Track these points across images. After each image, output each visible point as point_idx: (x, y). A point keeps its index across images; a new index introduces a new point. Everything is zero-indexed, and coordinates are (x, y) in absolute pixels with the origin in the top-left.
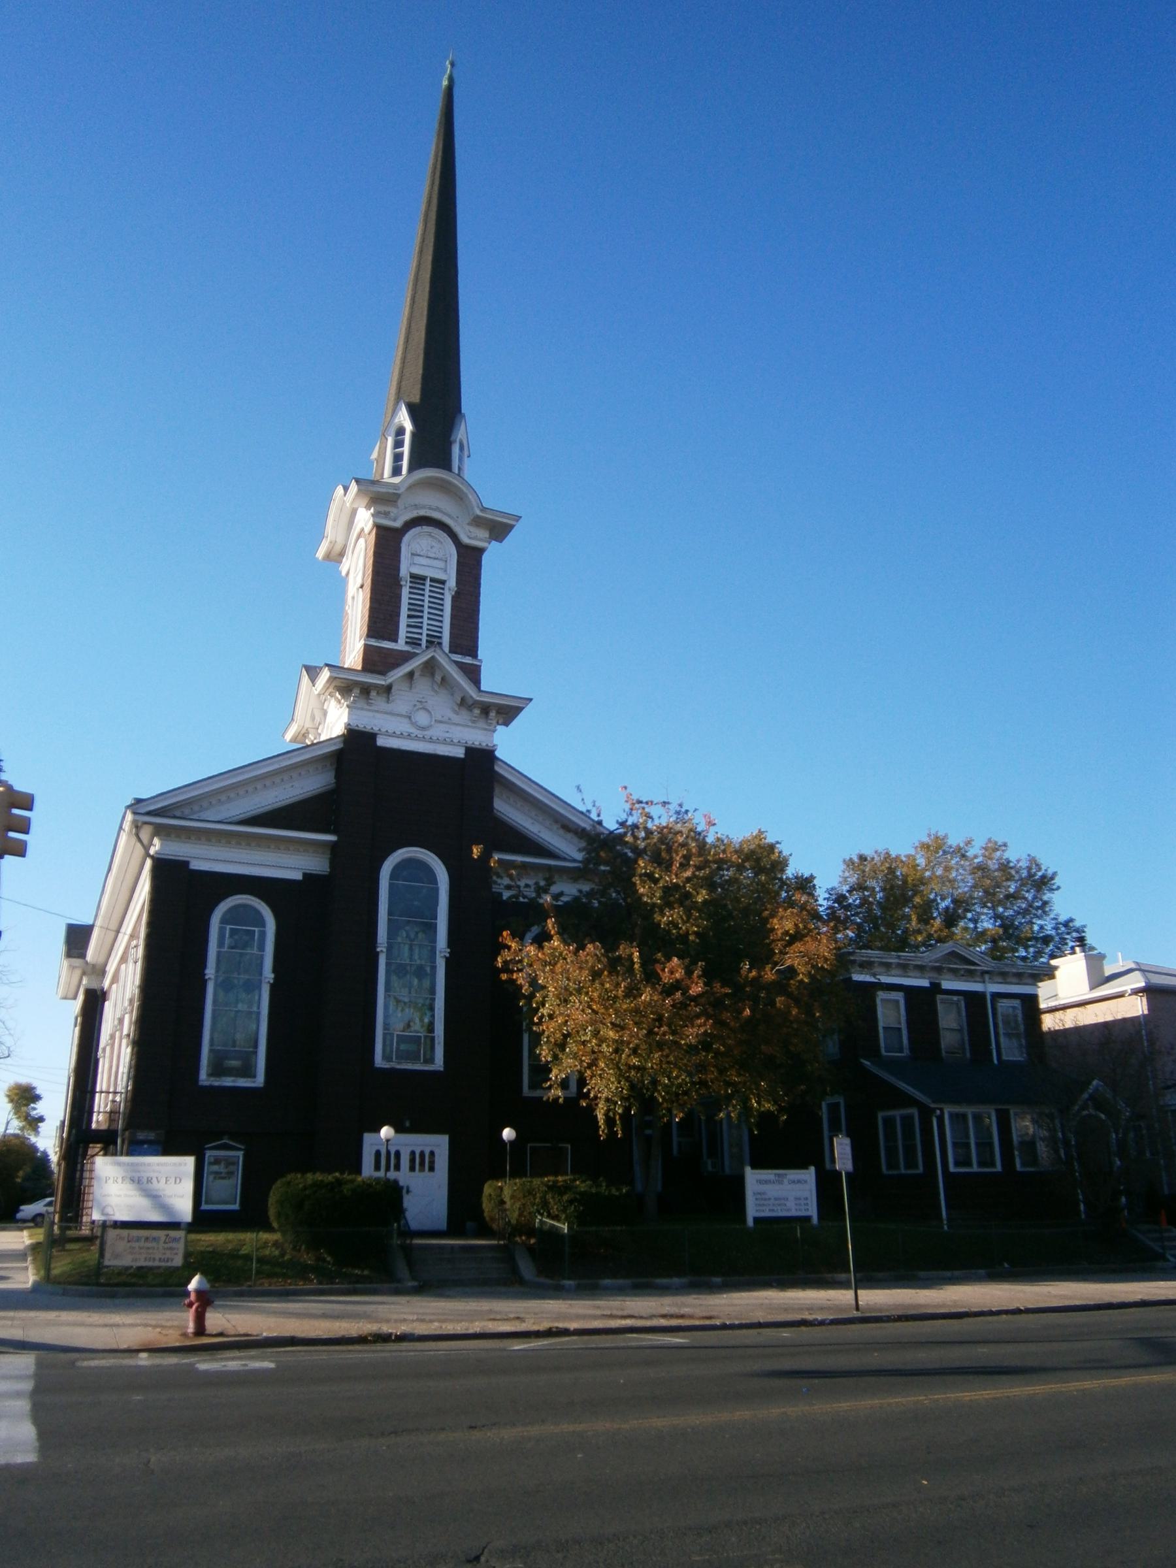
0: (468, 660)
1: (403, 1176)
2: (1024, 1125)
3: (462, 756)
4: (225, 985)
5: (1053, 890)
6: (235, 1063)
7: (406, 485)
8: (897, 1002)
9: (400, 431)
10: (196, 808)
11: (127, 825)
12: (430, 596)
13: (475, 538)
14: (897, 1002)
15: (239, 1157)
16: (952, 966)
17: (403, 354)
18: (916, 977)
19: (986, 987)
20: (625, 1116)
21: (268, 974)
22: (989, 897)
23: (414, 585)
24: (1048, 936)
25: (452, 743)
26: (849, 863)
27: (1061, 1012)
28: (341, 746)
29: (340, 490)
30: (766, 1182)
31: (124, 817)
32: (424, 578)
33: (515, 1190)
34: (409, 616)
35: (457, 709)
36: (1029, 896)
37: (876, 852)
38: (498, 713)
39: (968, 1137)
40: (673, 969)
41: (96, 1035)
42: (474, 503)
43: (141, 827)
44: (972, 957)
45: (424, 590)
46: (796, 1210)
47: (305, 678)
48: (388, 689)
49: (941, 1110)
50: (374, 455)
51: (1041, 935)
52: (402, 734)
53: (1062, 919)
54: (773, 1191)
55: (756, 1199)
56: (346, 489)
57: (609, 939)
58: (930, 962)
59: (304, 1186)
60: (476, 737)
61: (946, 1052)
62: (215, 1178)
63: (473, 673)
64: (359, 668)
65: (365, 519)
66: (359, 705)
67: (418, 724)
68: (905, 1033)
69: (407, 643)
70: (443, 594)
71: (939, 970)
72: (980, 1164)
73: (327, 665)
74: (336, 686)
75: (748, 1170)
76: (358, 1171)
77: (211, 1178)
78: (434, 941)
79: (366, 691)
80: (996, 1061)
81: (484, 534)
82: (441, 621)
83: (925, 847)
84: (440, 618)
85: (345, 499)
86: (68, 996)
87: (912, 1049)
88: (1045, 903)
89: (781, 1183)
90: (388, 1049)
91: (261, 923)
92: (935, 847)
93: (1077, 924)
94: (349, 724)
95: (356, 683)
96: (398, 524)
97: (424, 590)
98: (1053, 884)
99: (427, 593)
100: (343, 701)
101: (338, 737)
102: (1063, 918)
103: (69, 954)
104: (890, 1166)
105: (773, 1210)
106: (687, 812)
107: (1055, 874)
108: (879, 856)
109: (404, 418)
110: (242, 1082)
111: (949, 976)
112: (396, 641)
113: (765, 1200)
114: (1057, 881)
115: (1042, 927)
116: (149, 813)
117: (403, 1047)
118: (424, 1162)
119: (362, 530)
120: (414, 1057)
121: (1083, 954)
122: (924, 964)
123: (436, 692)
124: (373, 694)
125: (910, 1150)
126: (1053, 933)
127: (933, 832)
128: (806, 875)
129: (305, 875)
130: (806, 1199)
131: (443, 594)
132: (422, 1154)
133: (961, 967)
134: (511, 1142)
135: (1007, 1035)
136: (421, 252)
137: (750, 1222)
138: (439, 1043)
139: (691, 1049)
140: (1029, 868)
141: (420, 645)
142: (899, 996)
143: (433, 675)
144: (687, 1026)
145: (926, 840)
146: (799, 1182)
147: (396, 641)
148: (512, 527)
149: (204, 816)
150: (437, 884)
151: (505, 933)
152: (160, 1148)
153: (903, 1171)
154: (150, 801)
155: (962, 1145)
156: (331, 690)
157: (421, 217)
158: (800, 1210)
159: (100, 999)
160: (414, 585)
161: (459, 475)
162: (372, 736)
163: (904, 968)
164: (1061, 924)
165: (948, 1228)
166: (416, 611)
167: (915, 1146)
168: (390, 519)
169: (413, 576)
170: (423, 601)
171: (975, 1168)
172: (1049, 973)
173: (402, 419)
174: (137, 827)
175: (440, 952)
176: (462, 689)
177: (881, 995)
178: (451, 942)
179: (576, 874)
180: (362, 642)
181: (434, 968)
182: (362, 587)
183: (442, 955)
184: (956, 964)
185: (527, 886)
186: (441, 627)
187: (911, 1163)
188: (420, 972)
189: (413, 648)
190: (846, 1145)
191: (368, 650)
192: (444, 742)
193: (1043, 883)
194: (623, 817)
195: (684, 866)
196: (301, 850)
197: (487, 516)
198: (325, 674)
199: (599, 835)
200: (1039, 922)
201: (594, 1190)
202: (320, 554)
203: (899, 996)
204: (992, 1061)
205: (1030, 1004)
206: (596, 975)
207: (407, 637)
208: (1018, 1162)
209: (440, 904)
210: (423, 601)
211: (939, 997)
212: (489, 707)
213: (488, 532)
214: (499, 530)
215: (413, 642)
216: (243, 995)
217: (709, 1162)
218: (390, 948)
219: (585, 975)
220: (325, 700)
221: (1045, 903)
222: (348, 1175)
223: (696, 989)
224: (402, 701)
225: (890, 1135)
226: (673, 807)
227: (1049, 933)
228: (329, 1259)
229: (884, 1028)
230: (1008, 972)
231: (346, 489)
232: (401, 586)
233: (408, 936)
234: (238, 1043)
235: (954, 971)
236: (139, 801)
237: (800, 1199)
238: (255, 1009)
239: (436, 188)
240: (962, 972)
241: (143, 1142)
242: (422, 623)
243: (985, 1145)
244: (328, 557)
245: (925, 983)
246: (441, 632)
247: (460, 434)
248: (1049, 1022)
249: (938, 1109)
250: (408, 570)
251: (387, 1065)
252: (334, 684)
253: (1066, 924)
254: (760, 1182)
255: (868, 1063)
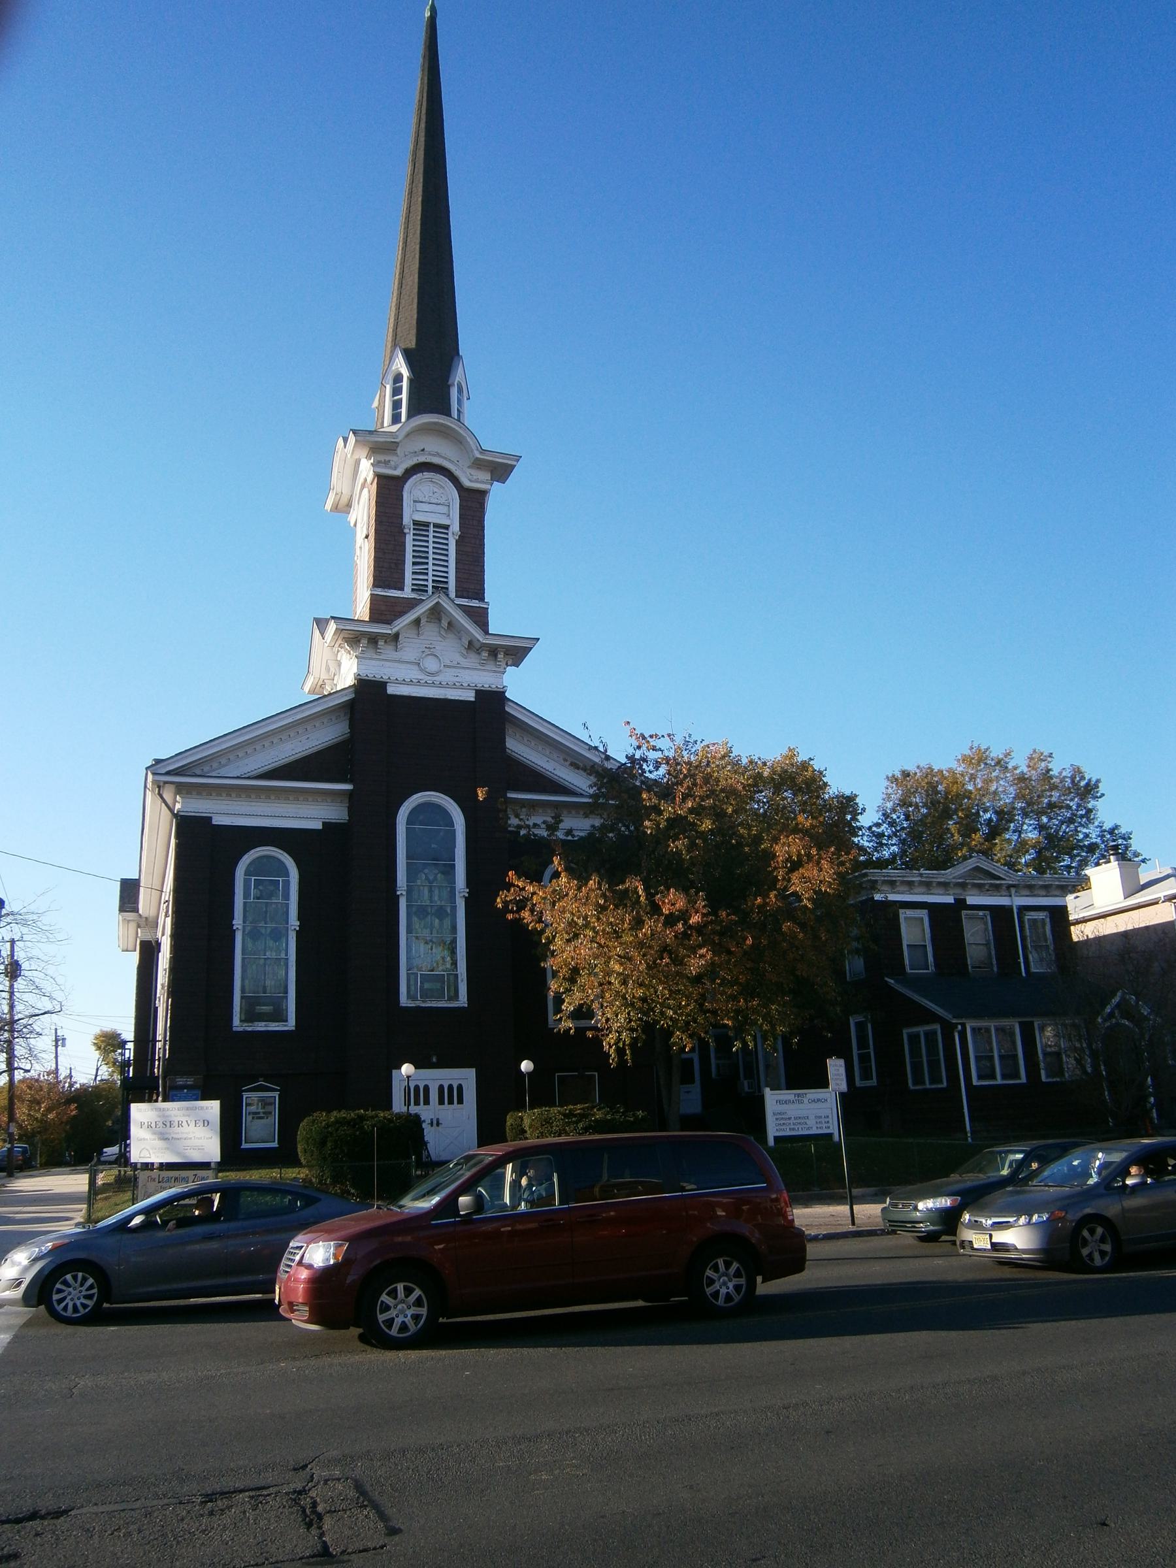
0: (475, 603)
1: (426, 1113)
2: (1047, 1036)
4: (253, 935)
5: (1097, 797)
6: (266, 1009)
7: (404, 433)
8: (922, 919)
9: (398, 378)
10: (215, 765)
11: (149, 785)
12: (434, 542)
13: (477, 481)
14: (922, 919)
15: (275, 1097)
16: (976, 881)
17: (397, 300)
18: (939, 894)
19: (1012, 901)
20: (633, 1045)
21: (294, 922)
22: (1032, 808)
23: (418, 532)
24: (1093, 844)
25: (462, 687)
26: (893, 779)
27: (1103, 920)
28: (353, 696)
29: (341, 441)
31: (146, 779)
32: (427, 525)
33: (533, 1120)
34: (414, 564)
35: (465, 653)
36: (1073, 804)
37: (918, 767)
38: (506, 654)
39: (991, 1050)
41: (154, 983)
42: (474, 447)
43: (163, 787)
44: (997, 871)
45: (428, 536)
47: (317, 633)
48: (396, 637)
49: (964, 1025)
50: (376, 404)
51: (1086, 843)
52: (411, 681)
53: (1107, 826)
54: (793, 1110)
55: (777, 1119)
56: (345, 440)
57: (614, 872)
58: (954, 878)
59: (327, 1124)
60: (486, 679)
61: (973, 967)
62: (253, 1118)
63: (480, 618)
64: (367, 619)
65: (367, 469)
66: (367, 655)
67: (427, 670)
68: (929, 949)
69: (413, 590)
70: (447, 539)
71: (963, 886)
72: (1004, 1077)
73: (333, 618)
75: (767, 1091)
76: (388, 1105)
77: (250, 1118)
78: (452, 881)
79: (373, 640)
80: (1024, 974)
81: (486, 476)
82: (447, 567)
83: (966, 759)
84: (446, 564)
85: (346, 450)
86: (129, 949)
87: (936, 965)
88: (1089, 811)
90: (413, 988)
91: (286, 873)
92: (979, 758)
93: (1123, 830)
94: (359, 675)
95: (364, 634)
96: (399, 472)
97: (428, 536)
98: (1097, 792)
99: (431, 539)
100: (352, 652)
101: (350, 687)
102: (1107, 826)
103: (122, 909)
104: (918, 1080)
105: (793, 1129)
106: (696, 742)
107: (1098, 781)
108: (921, 771)
109: (401, 365)
110: (274, 1027)
111: (975, 891)
112: (402, 589)
113: (786, 1119)
114: (1102, 788)
115: (1087, 836)
116: (168, 773)
117: (427, 986)
118: (451, 1095)
119: (366, 480)
120: (440, 996)
121: (1117, 862)
122: (947, 881)
123: (444, 638)
124: (381, 643)
125: (934, 1065)
126: (1098, 840)
127: (975, 745)
128: (848, 793)
129: (324, 824)
130: (828, 1117)
131: (447, 539)
132: (451, 1087)
133: (986, 882)
134: (529, 1074)
135: (1036, 948)
136: (411, 193)
137: (771, 1142)
138: (462, 981)
139: (697, 979)
140: (1073, 778)
141: (427, 591)
142: (923, 914)
143: (440, 620)
144: (690, 957)
145: (968, 752)
147: (402, 589)
148: (513, 467)
149: (223, 772)
150: (454, 826)
151: (510, 873)
152: (199, 1092)
153: (928, 1086)
154: (170, 761)
155: (985, 1059)
156: (339, 641)
157: (409, 157)
159: (156, 950)
160: (418, 532)
161: (459, 420)
162: (383, 685)
163: (927, 885)
164: (1105, 831)
165: (972, 1139)
166: (421, 558)
167: (939, 1060)
168: (391, 468)
169: (416, 523)
170: (427, 547)
171: (999, 1081)
172: (1080, 884)
173: (399, 366)
174: (159, 787)
175: (460, 892)
176: (468, 632)
177: (904, 914)
178: (469, 882)
179: (589, 810)
180: (369, 592)
181: (454, 908)
182: (367, 537)
183: (462, 895)
184: (981, 879)
185: (535, 825)
186: (447, 572)
187: (935, 1079)
188: (441, 913)
189: (420, 595)
190: (841, 1066)
191: (374, 599)
192: (454, 686)
193: (1089, 790)
194: (631, 751)
195: (685, 797)
196: (310, 799)
197: (486, 458)
198: (332, 627)
199: (606, 770)
200: (1085, 830)
201: (609, 1117)
202: (328, 506)
203: (923, 914)
204: (1021, 973)
205: (1059, 916)
206: (602, 909)
207: (413, 585)
208: (1043, 1073)
209: (457, 846)
210: (427, 547)
211: (964, 912)
212: (496, 649)
213: (489, 474)
214: (501, 470)
215: (419, 589)
216: (271, 943)
217: (746, 1083)
218: (409, 891)
219: (591, 911)
220: (338, 651)
221: (1089, 811)
222: (372, 1111)
223: (695, 919)
224: (411, 648)
225: (915, 1052)
226: (679, 740)
227: (1094, 840)
228: (353, 1191)
229: (908, 945)
230: (1035, 885)
231: (345, 440)
232: (405, 534)
233: (427, 878)
234: (268, 989)
235: (980, 887)
236: (158, 762)
237: (821, 1117)
238: (283, 956)
239: (423, 125)
240: (987, 887)
241: (182, 1087)
242: (427, 569)
243: (1009, 1059)
244: (336, 508)
245: (950, 899)
246: (447, 577)
247: (458, 377)
248: (1077, 933)
249: (960, 1024)
250: (411, 517)
251: (412, 1004)
252: (342, 636)
253: (1112, 831)
254: (779, 1102)
255: (892, 981)
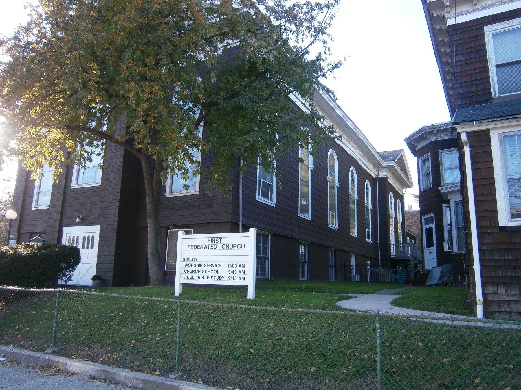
3: (445, 251)
30: (198, 247)
40: (61, 153)
46: (230, 278)
74: (409, 260)
89: (214, 247)
127: (332, 73)
146: (235, 246)
158: (234, 278)
237: (235, 266)
